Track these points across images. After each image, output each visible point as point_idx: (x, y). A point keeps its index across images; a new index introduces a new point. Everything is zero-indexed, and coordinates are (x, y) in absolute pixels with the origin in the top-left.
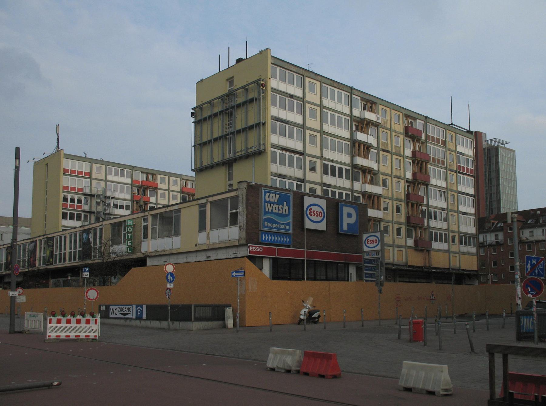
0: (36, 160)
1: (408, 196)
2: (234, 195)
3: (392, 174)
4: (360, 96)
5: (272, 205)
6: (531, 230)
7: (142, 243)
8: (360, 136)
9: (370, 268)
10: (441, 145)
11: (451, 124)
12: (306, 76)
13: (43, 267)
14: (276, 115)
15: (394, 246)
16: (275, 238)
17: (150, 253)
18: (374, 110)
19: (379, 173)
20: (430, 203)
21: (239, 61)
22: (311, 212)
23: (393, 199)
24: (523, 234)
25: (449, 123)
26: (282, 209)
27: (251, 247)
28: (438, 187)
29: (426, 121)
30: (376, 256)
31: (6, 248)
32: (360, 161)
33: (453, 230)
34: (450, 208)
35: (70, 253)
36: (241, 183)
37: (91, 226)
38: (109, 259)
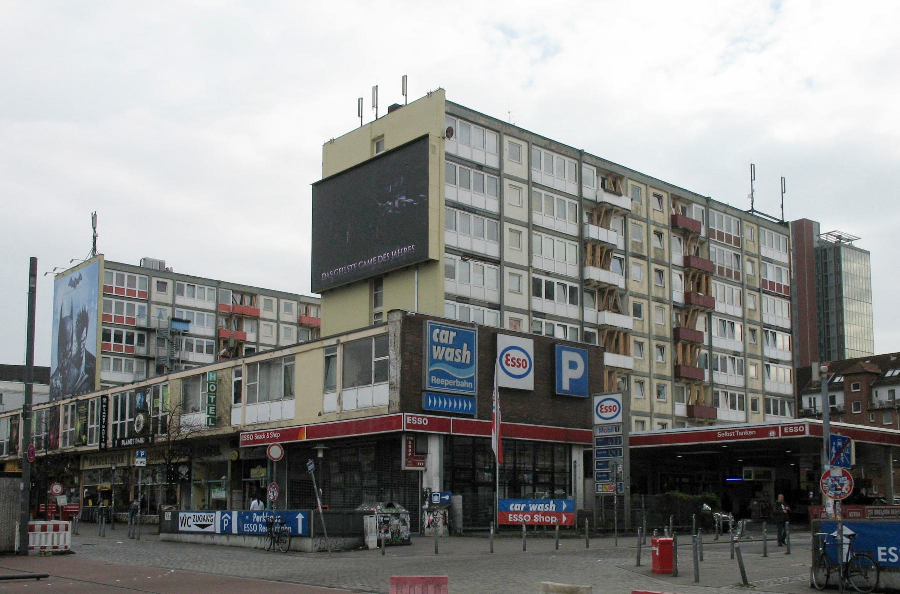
0: (59, 271)
1: (676, 332)
2: (382, 333)
3: (649, 296)
4: (596, 165)
5: (444, 349)
6: (891, 388)
7: (233, 410)
8: (595, 232)
9: (606, 452)
10: (733, 245)
11: (750, 211)
12: (505, 134)
13: (70, 449)
14: (454, 199)
15: (653, 415)
16: (443, 401)
17: (245, 427)
18: (619, 188)
19: (628, 293)
20: (714, 345)
21: (393, 108)
22: (509, 360)
23: (651, 336)
24: (877, 396)
25: (747, 208)
26: (461, 355)
27: (409, 418)
28: (729, 317)
29: (709, 205)
30: (615, 433)
31: (10, 418)
32: (595, 274)
33: (755, 388)
34: (748, 351)
35: (115, 426)
36: (393, 314)
37: (150, 382)
38: (179, 436)
